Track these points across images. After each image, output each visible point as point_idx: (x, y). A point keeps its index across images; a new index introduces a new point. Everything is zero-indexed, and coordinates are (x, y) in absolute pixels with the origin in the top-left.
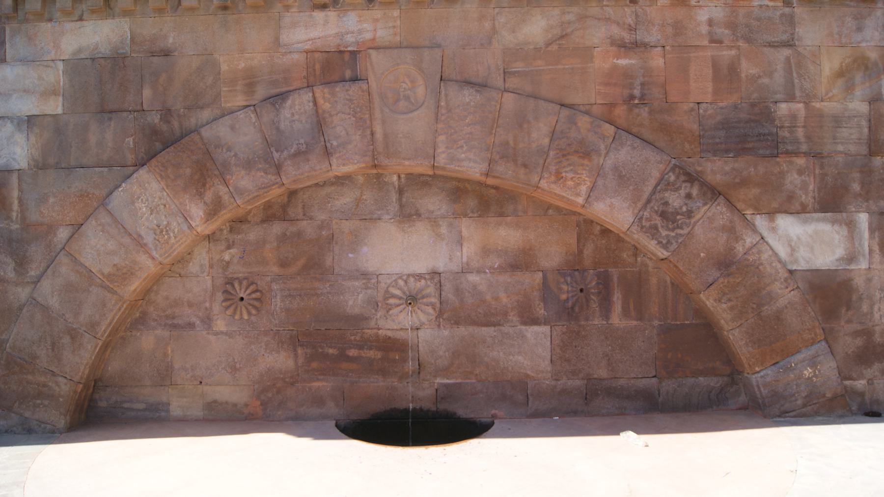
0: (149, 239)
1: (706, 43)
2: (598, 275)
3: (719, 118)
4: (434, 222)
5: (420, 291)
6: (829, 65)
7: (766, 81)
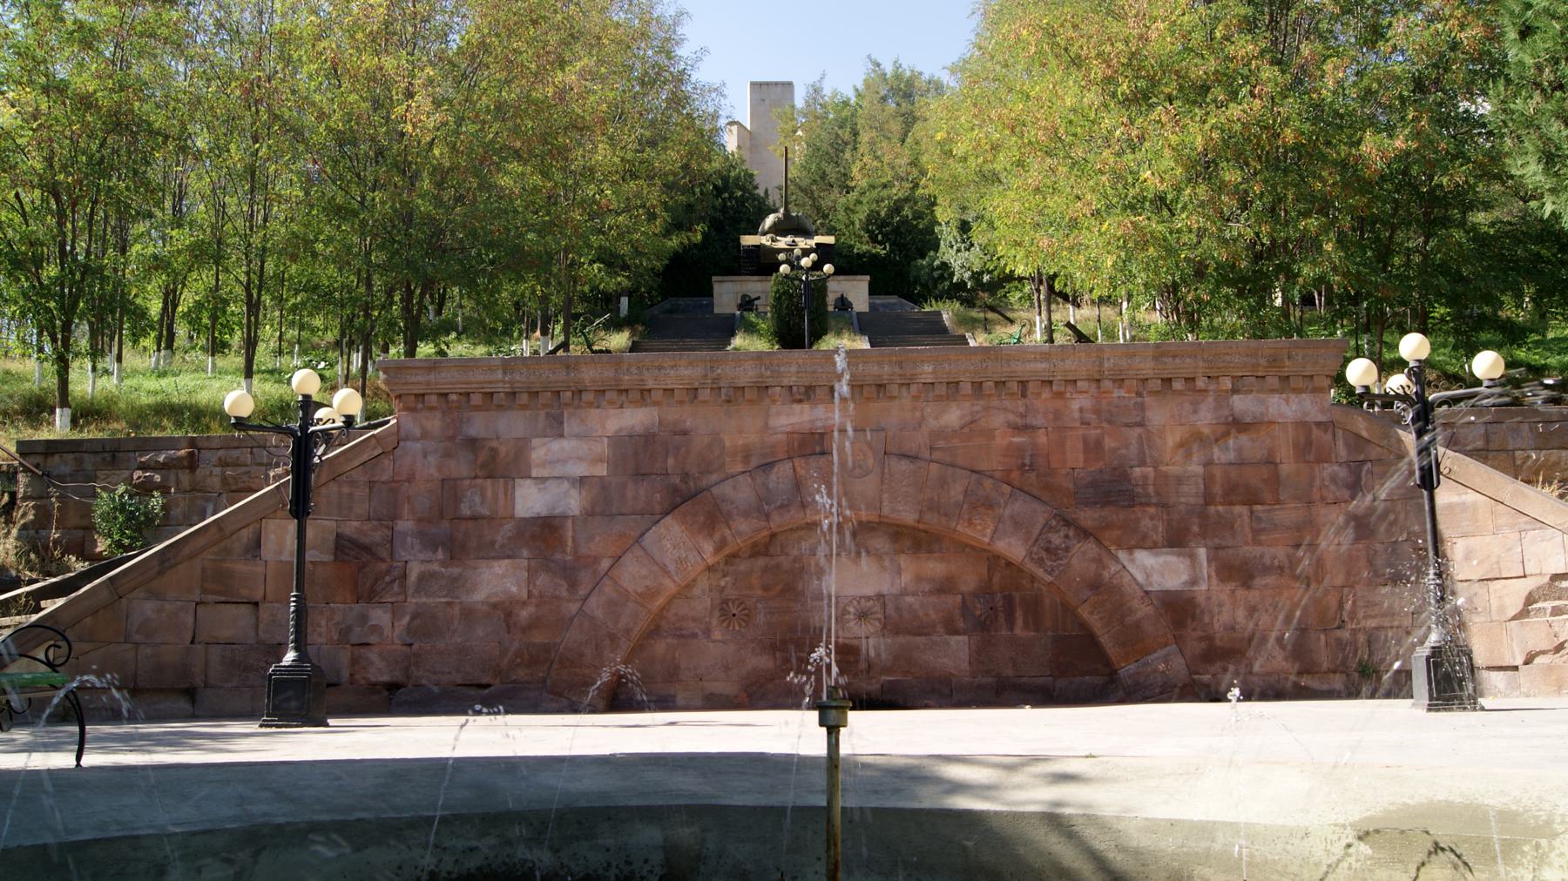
0: (672, 568)
1: (1078, 425)
2: (1004, 597)
3: (1089, 479)
4: (879, 557)
5: (870, 609)
6: (1172, 439)
7: (1123, 451)
